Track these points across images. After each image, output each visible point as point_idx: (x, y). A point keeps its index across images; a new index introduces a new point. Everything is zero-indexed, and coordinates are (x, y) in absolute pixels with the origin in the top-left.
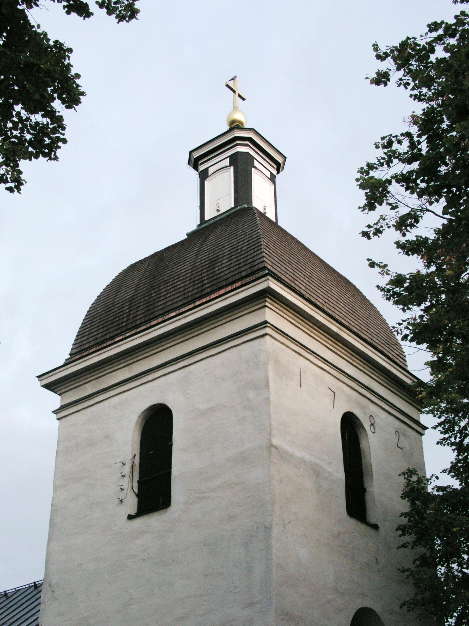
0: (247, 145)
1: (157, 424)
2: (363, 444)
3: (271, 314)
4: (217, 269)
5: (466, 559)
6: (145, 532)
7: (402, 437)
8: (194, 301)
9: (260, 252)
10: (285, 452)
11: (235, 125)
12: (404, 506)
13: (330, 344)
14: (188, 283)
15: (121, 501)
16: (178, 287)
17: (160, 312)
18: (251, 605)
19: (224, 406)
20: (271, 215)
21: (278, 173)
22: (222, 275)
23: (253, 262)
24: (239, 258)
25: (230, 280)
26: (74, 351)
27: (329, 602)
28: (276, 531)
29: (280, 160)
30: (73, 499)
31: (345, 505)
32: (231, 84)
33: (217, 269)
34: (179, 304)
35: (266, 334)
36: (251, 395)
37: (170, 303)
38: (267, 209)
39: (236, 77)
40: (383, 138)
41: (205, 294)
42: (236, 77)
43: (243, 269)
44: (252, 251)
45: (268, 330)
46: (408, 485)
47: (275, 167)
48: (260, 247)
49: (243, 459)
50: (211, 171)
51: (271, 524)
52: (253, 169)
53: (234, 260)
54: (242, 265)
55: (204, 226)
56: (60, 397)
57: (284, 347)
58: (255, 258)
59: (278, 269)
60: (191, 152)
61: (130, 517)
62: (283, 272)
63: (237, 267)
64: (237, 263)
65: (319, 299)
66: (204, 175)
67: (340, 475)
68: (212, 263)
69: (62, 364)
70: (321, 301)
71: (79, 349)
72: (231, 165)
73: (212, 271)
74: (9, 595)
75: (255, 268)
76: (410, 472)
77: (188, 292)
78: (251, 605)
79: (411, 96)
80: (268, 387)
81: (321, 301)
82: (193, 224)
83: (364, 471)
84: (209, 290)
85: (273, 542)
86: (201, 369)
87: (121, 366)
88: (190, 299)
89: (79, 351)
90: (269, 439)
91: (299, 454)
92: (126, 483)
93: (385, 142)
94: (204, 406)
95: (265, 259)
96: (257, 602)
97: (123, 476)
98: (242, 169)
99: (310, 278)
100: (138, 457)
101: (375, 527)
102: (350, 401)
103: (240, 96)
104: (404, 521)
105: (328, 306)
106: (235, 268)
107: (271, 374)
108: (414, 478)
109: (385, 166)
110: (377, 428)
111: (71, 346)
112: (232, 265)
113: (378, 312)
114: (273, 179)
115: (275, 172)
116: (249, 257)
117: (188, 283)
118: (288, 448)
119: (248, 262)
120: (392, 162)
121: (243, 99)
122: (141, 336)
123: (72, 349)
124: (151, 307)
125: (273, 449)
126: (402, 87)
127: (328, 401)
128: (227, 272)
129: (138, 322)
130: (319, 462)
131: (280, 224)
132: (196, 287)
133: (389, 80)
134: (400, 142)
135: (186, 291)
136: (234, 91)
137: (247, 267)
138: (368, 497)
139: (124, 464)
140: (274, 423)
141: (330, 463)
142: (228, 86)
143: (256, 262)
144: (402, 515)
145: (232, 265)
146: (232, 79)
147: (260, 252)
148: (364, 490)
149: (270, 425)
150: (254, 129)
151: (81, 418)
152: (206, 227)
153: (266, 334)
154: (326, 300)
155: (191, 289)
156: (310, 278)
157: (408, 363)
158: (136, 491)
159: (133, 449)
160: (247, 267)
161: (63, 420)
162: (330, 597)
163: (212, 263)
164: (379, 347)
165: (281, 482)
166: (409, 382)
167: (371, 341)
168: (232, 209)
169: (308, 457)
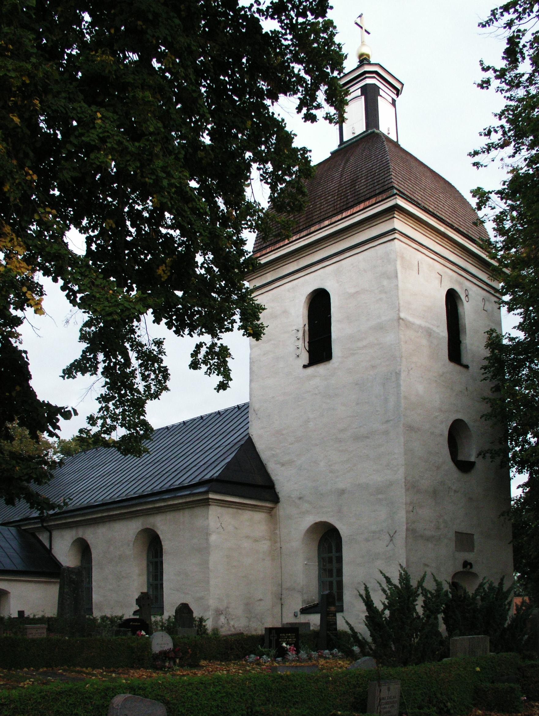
0: (374, 77)
1: (319, 303)
2: (460, 310)
3: (398, 223)
4: (357, 187)
6: (316, 376)
7: (487, 303)
8: (341, 212)
9: (388, 174)
10: (409, 322)
12: (487, 353)
13: (438, 240)
14: (336, 197)
15: (298, 356)
16: (329, 201)
17: (316, 220)
18: (387, 421)
19: (367, 291)
20: (393, 137)
21: (398, 97)
22: (361, 191)
23: (384, 182)
25: (368, 196)
26: (255, 249)
27: (436, 417)
28: (403, 375)
29: (399, 86)
30: (264, 354)
31: (447, 354)
32: (358, 21)
33: (357, 187)
34: (330, 214)
35: (395, 238)
36: (385, 283)
37: (323, 213)
38: (390, 130)
39: (362, 14)
40: (485, 129)
41: (350, 207)
42: (362, 14)
43: (377, 187)
44: (383, 174)
45: (396, 236)
46: (489, 339)
47: (395, 93)
48: (388, 171)
49: (380, 328)
51: (400, 371)
52: (379, 98)
54: (376, 184)
55: (343, 146)
57: (407, 246)
58: (386, 179)
59: (403, 187)
61: (305, 367)
62: (405, 189)
64: (371, 183)
65: (431, 206)
68: (354, 182)
70: (432, 207)
71: (259, 248)
72: (362, 95)
74: (222, 413)
75: (386, 187)
76: (492, 331)
77: (337, 205)
78: (387, 421)
79: (505, 97)
80: (397, 277)
81: (432, 207)
83: (461, 329)
84: (352, 203)
85: (402, 382)
87: (292, 260)
88: (338, 210)
90: (399, 314)
91: (418, 322)
92: (300, 343)
93: (486, 131)
94: (353, 291)
95: (393, 180)
96: (391, 420)
97: (298, 339)
99: (424, 190)
101: (467, 367)
102: (451, 280)
103: (366, 31)
104: (486, 363)
105: (437, 210)
107: (399, 267)
108: (494, 335)
109: (486, 153)
112: (368, 184)
114: (394, 103)
115: (395, 97)
116: (381, 178)
117: (336, 197)
118: (411, 319)
120: (491, 150)
121: (369, 33)
123: (254, 248)
124: (310, 216)
125: (401, 321)
126: (499, 92)
127: (437, 282)
128: (365, 190)
129: (301, 228)
130: (431, 327)
131: (399, 143)
132: (342, 201)
133: (490, 85)
134: (496, 132)
135: (335, 204)
136: (362, 28)
137: (380, 186)
138: (463, 347)
139: (298, 331)
140: (401, 302)
141: (438, 327)
142: (356, 23)
143: (386, 183)
144: (485, 358)
145: (368, 184)
146: (360, 16)
147: (388, 174)
148: (460, 342)
149: (399, 304)
150: (379, 64)
152: (345, 147)
153: (395, 238)
154: (436, 206)
155: (339, 202)
156: (424, 190)
159: (303, 321)
160: (380, 186)
162: (437, 414)
163: (354, 182)
165: (406, 343)
167: (467, 233)
168: (364, 132)
169: (423, 323)
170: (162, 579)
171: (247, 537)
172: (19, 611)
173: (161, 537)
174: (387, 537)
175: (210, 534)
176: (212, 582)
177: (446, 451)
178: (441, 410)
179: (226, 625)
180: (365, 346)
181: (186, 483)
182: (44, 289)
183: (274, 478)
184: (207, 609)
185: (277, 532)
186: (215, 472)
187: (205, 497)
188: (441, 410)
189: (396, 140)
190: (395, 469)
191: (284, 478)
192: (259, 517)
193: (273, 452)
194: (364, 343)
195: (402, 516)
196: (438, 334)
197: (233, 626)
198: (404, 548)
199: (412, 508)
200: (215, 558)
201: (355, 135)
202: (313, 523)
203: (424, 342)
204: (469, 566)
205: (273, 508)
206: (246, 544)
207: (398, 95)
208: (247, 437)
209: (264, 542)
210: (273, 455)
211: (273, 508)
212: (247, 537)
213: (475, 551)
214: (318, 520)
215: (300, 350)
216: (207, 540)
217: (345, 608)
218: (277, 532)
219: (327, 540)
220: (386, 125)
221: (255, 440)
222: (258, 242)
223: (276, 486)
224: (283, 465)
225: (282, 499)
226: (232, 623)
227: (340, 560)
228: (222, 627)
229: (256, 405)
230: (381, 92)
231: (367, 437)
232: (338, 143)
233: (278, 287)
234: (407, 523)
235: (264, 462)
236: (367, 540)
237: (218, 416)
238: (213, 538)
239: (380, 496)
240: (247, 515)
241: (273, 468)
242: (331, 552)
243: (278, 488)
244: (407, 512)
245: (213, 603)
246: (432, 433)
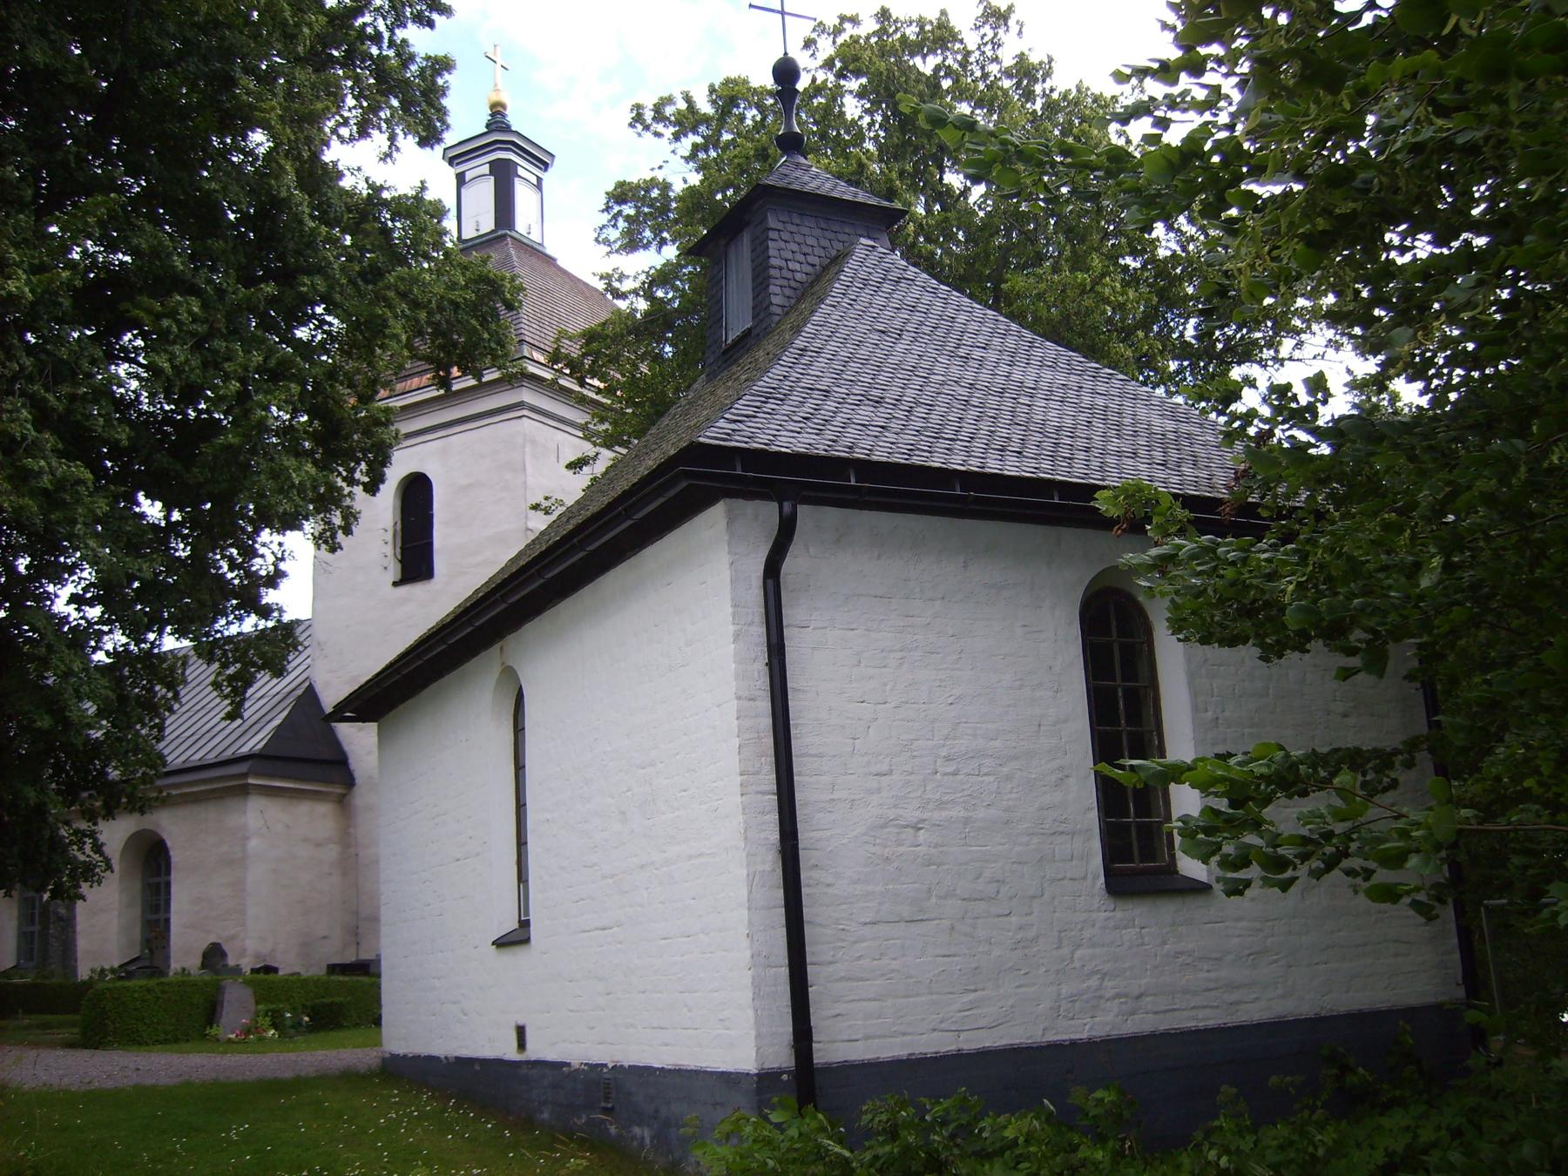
50: (468, 176)
61: (395, 584)
86: (461, 440)
92: (389, 550)
98: (503, 176)
114: (539, 186)
170: (168, 909)
171: (306, 840)
173: (169, 844)
181: (211, 758)
182: (633, 178)
183: (346, 748)
184: (243, 953)
192: (324, 809)
200: (256, 874)
205: (344, 796)
212: (306, 840)
220: (525, 218)
221: (318, 688)
223: (351, 761)
229: (319, 632)
233: (521, 843)
238: (253, 843)
240: (304, 809)
243: (354, 764)
245: (252, 945)
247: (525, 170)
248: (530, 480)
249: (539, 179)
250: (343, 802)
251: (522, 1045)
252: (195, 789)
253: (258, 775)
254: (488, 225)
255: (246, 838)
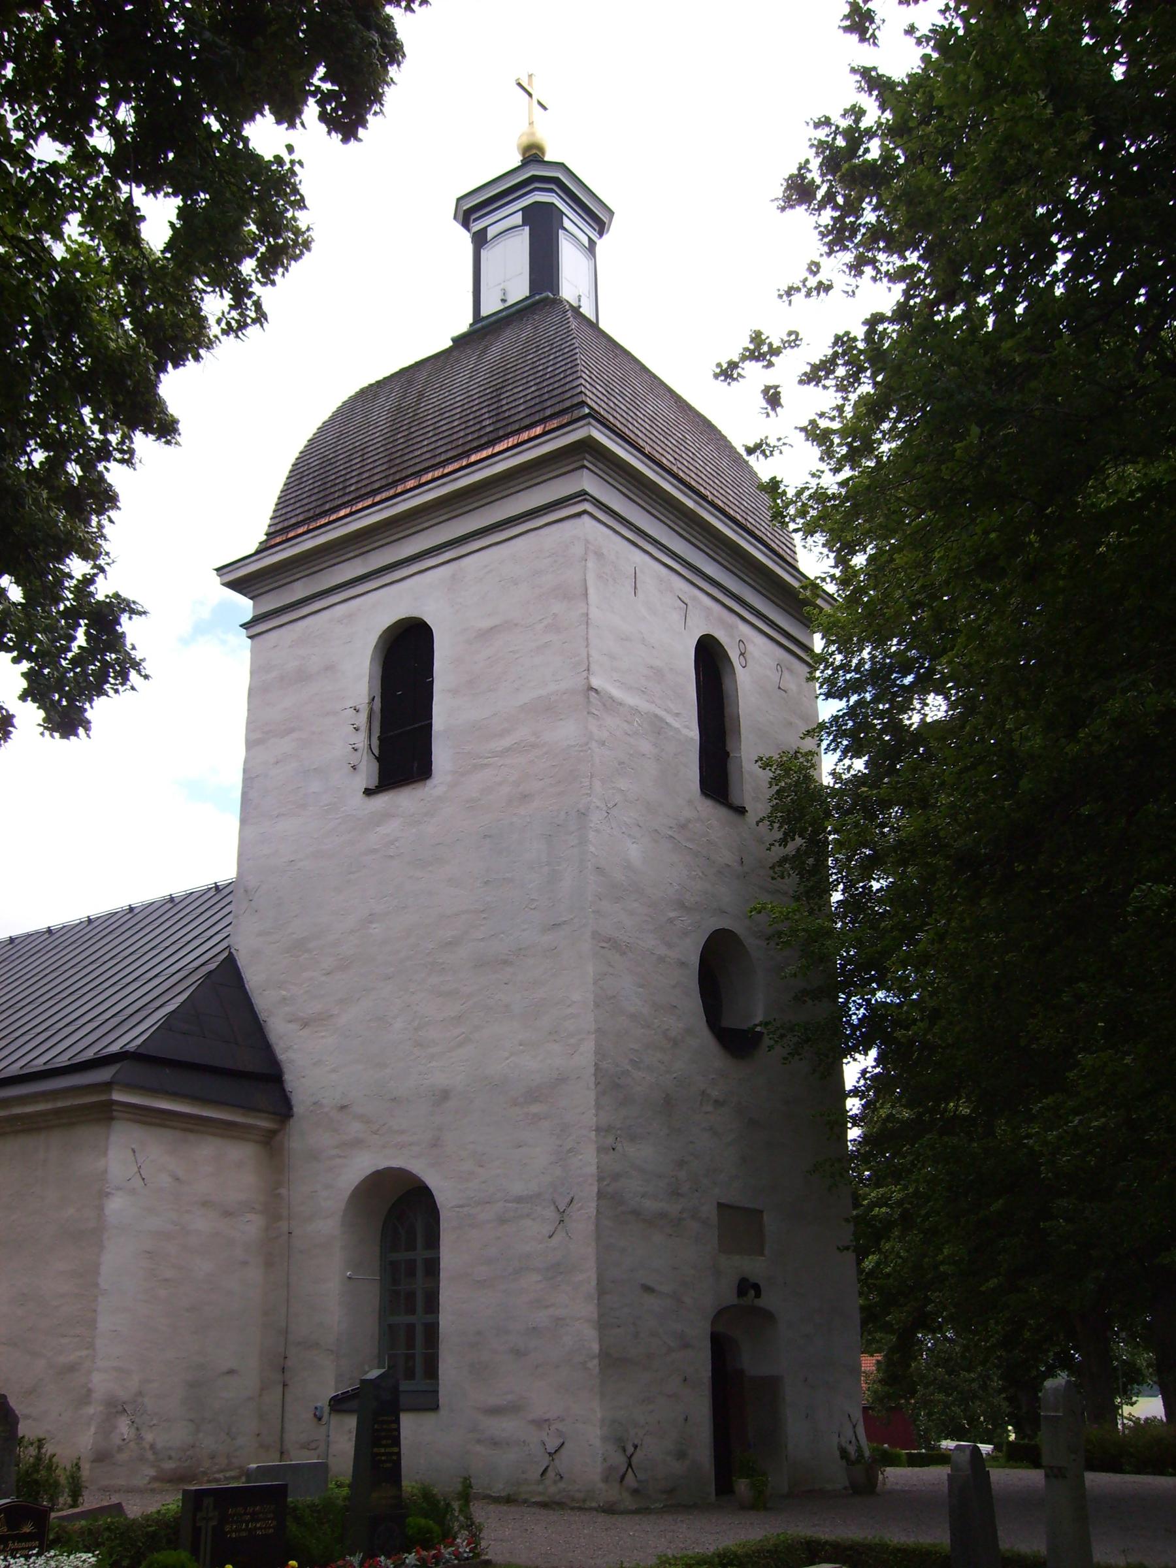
0: (551, 191)
4: (504, 402)
5: (12, 133)
7: (786, 675)
8: (467, 454)
9: (575, 376)
11: (533, 154)
19: (516, 625)
20: (587, 310)
24: (541, 386)
25: (527, 422)
26: (272, 530)
28: (595, 818)
49: (547, 709)
50: (491, 233)
53: (533, 389)
55: (479, 325)
56: (251, 602)
60: (459, 200)
61: (368, 792)
63: (537, 400)
64: (537, 394)
66: (480, 240)
67: (693, 732)
69: (252, 551)
71: (279, 527)
72: (524, 224)
73: (495, 406)
74: (177, 900)
75: (568, 404)
80: (586, 594)
82: (462, 322)
85: (591, 835)
86: (477, 564)
89: (279, 533)
91: (631, 700)
92: (361, 739)
96: (565, 922)
97: (357, 729)
98: (543, 232)
100: (378, 700)
106: (533, 403)
110: (749, 661)
111: (268, 522)
113: (756, 474)
114: (591, 248)
118: (616, 693)
119: (555, 393)
121: (545, 108)
122: (382, 510)
127: (676, 617)
131: (602, 325)
136: (530, 95)
141: (677, 715)
142: (519, 85)
143: (569, 395)
147: (575, 376)
149: (588, 656)
150: (563, 164)
151: (285, 638)
152: (483, 328)
153: (585, 512)
157: (798, 557)
158: (376, 752)
161: (257, 639)
162: (672, 915)
164: (757, 532)
166: (796, 584)
168: (527, 298)
172: (435, 1408)
174: (550, 1213)
175: (108, 1194)
176: (105, 1323)
177: (694, 1004)
178: (681, 905)
179: (132, 1445)
180: (508, 750)
183: (282, 1056)
185: (283, 1191)
186: (132, 1038)
187: (103, 1098)
188: (681, 905)
189: (593, 319)
190: (572, 1041)
191: (314, 1062)
193: (284, 993)
194: (507, 742)
195: (587, 1160)
196: (677, 730)
197: (152, 1447)
198: (593, 1244)
199: (610, 1136)
200: (118, 1260)
201: (507, 305)
202: (369, 1172)
203: (645, 746)
204: (752, 1292)
205: (272, 1133)
206: (202, 1223)
207: (601, 234)
208: (225, 954)
209: (249, 1217)
210: (284, 999)
211: (272, 1133)
212: (205, 1204)
213: (766, 1252)
214: (383, 1164)
215: (359, 754)
216: (101, 1208)
217: (442, 1401)
218: (283, 1191)
219: (401, 1216)
220: (572, 282)
221: (242, 961)
222: (279, 513)
223: (288, 1077)
224: (305, 1024)
225: (298, 1109)
226: (149, 1437)
227: (433, 1268)
228: (120, 1449)
230: (567, 223)
231: (505, 962)
232: (470, 319)
234: (600, 1179)
235: (262, 1016)
236: (502, 1220)
237: (169, 905)
238: (116, 1205)
239: (535, 1108)
240: (207, 1149)
241: (282, 1032)
242: (414, 1249)
243: (291, 1079)
244: (600, 1150)
246: (661, 959)
247: (572, 223)
248: (594, 613)
249: (592, 243)
250: (272, 1144)
251: (109, 517)
252: (29, 1109)
253: (130, 1087)
254: (519, 290)
255: (104, 1195)
